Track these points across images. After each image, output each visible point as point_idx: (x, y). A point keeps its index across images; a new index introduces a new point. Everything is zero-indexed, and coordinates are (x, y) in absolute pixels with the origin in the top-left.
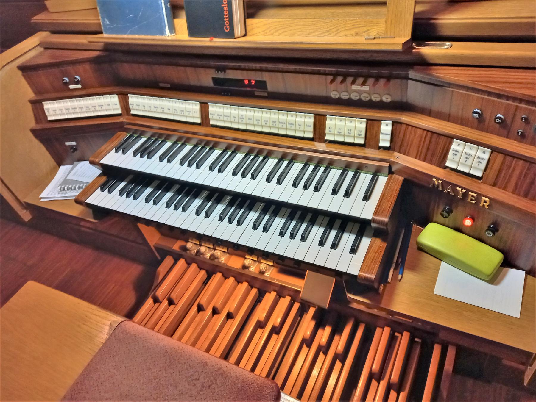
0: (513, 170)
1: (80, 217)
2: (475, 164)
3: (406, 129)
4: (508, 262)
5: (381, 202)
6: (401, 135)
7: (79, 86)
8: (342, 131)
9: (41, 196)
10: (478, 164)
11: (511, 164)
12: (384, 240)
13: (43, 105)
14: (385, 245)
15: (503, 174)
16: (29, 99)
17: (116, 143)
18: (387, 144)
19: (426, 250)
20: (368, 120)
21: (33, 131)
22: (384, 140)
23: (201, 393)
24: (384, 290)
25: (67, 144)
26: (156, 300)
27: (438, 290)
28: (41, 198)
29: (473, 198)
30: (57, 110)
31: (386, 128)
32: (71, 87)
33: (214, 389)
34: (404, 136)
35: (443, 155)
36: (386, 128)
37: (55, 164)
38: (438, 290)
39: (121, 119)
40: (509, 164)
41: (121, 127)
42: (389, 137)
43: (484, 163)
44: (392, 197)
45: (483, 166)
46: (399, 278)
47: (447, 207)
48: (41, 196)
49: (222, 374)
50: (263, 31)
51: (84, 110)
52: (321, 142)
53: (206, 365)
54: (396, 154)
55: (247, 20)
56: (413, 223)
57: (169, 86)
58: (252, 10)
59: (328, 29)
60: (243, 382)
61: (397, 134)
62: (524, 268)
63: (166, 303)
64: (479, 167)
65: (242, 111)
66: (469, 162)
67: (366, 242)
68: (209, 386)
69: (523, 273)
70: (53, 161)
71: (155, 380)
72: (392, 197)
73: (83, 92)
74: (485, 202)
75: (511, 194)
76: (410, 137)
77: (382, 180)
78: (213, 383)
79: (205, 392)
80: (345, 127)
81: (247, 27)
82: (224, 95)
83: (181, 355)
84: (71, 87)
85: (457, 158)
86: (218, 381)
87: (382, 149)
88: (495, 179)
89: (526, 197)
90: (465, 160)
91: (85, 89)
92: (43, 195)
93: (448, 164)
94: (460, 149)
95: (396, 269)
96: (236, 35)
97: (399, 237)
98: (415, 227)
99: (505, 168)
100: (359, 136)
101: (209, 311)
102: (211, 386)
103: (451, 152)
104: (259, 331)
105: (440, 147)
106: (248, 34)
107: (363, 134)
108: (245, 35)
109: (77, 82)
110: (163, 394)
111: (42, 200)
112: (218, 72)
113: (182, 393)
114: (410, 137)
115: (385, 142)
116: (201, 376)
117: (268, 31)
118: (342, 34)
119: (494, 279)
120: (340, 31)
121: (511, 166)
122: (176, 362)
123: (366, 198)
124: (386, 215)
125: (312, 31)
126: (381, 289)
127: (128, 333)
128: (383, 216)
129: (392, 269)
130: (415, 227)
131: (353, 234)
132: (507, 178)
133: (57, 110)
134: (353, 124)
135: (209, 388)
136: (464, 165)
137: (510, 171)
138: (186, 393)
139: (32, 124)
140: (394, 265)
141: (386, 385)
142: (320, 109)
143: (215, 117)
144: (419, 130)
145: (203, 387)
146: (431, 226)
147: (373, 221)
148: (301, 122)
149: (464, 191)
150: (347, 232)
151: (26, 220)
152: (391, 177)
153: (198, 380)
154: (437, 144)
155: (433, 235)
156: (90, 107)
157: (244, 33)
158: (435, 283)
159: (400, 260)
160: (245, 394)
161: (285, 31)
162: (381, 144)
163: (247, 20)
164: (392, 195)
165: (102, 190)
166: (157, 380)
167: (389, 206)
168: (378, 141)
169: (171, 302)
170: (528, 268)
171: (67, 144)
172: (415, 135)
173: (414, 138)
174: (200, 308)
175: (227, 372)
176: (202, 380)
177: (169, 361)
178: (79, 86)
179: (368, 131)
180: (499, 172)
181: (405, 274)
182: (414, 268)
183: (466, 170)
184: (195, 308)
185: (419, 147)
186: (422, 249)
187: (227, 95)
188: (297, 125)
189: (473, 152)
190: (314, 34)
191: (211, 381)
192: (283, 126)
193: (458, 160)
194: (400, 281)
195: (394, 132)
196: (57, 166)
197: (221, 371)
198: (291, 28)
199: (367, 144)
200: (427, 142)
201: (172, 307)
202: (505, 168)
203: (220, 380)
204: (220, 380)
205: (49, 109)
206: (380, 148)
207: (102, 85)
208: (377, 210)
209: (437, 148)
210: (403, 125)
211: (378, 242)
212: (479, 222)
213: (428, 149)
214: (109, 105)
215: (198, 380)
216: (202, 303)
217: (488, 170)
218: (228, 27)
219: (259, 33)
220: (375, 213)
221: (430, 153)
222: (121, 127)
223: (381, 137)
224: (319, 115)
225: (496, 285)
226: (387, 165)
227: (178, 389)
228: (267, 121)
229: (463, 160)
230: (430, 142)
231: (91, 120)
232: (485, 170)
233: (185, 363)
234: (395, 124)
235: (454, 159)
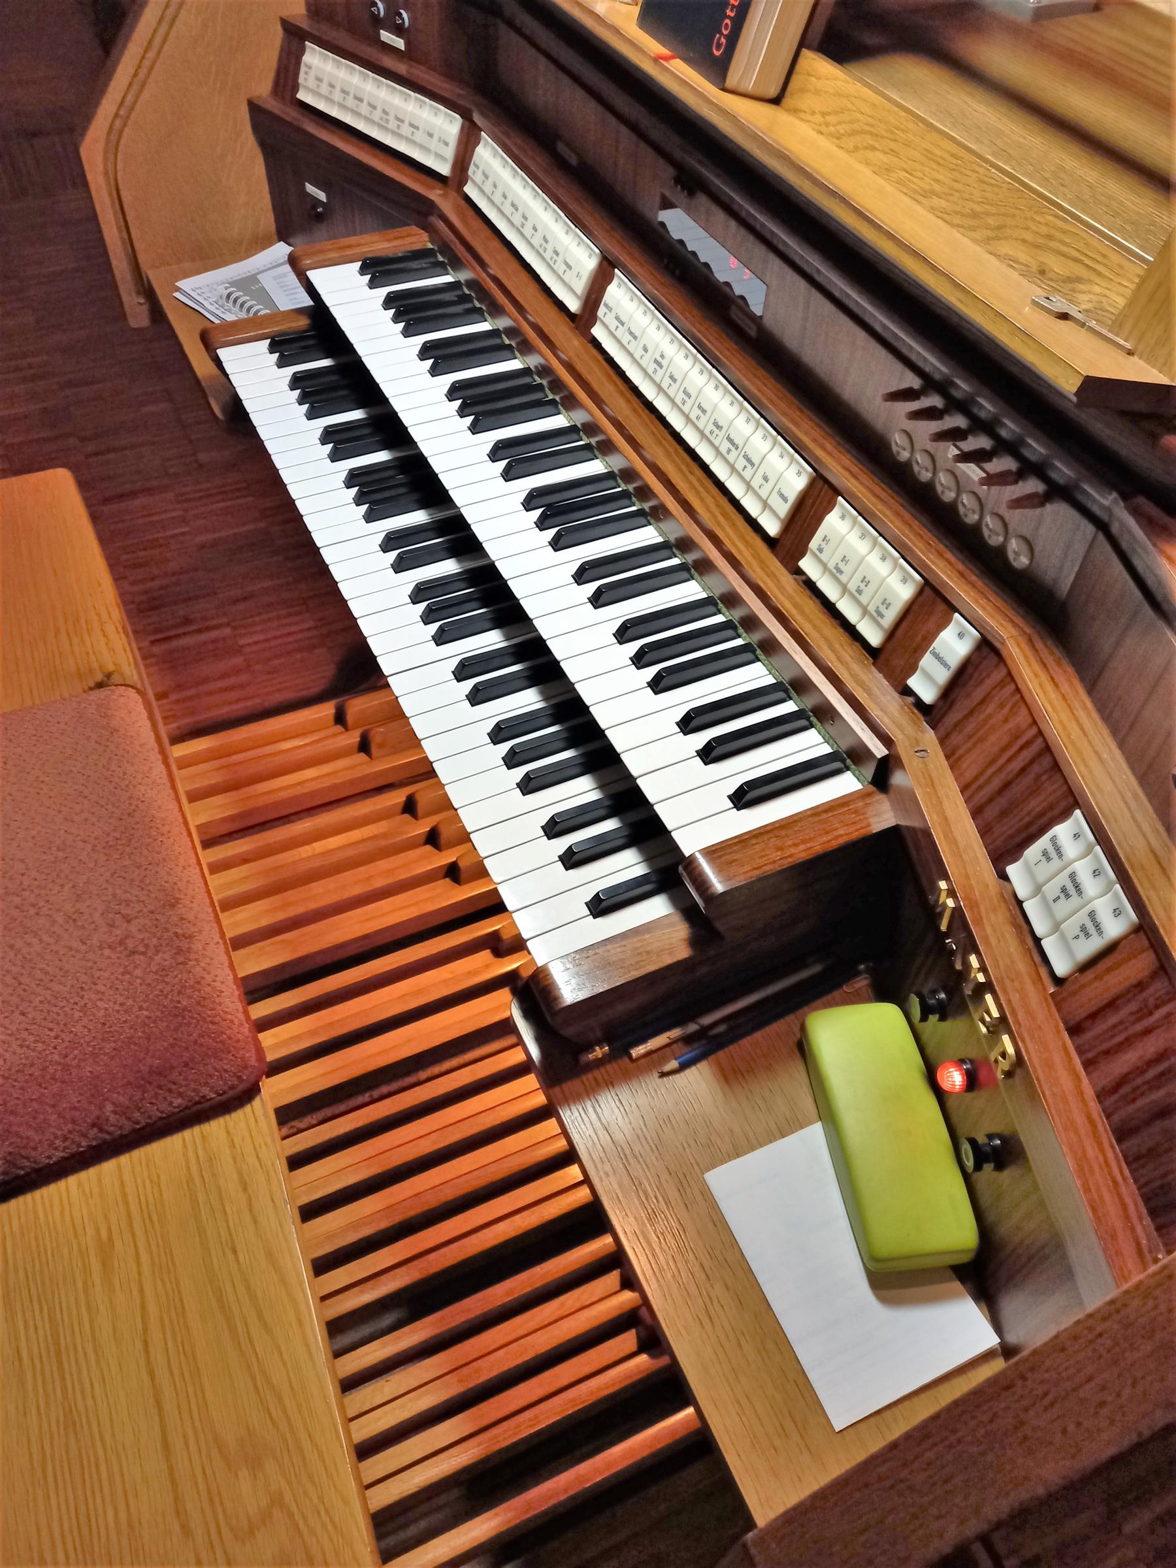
0: (1148, 1032)
1: (204, 384)
2: (1071, 927)
3: (1001, 684)
4: (983, 1274)
5: (755, 836)
6: (978, 694)
7: (400, 43)
8: (847, 569)
9: (179, 284)
10: (1077, 931)
11: (1157, 1007)
12: (695, 942)
13: (302, 51)
14: (683, 952)
15: (1113, 1019)
16: (285, 14)
17: (382, 245)
18: (928, 695)
19: (808, 1059)
20: (927, 582)
21: (254, 108)
22: (928, 676)
23: (107, 952)
24: (600, 1063)
25: (310, 188)
26: (340, 718)
27: (727, 1182)
28: (178, 289)
29: (988, 1019)
30: (334, 84)
31: (954, 643)
32: (386, 36)
33: (136, 967)
34: (982, 702)
35: (1024, 835)
36: (954, 643)
37: (273, 228)
38: (727, 1182)
39: (435, 195)
40: (1151, 1001)
41: (420, 211)
42: (942, 676)
43: (1094, 945)
44: (802, 847)
45: (1086, 949)
46: (668, 1067)
47: (943, 996)
48: (179, 284)
49: (179, 951)
50: (823, 114)
51: (377, 116)
52: (785, 567)
53: (173, 906)
54: (929, 737)
55: (805, 52)
56: (867, 971)
57: (574, 160)
58: (847, 32)
59: (978, 208)
60: (199, 1003)
61: (972, 682)
62: (1006, 1328)
63: (354, 738)
64: (1075, 944)
65: (863, 536)
66: (1063, 908)
67: (657, 908)
68: (133, 953)
69: (993, 1340)
70: (271, 217)
71: (59, 849)
72: (802, 847)
73: (402, 68)
74: (1004, 1055)
75: (1089, 1092)
76: (990, 717)
77: (846, 784)
78: (143, 953)
79: (114, 956)
80: (863, 564)
81: (794, 78)
82: (666, 268)
83: (148, 845)
84: (386, 36)
85: (1044, 871)
86: (158, 958)
87: (911, 700)
88: (1086, 1018)
89: (1119, 1140)
90: (1058, 892)
91: (411, 59)
92: (185, 284)
93: (1012, 870)
94: (1071, 849)
95: (687, 1040)
96: (732, 80)
97: (794, 971)
98: (862, 982)
99: (1133, 1007)
100: (875, 617)
101: (422, 828)
102: (136, 957)
103: (1043, 842)
104: (486, 955)
105: (1036, 804)
106: (787, 101)
107: (890, 617)
108: (776, 101)
109: (399, 31)
110: (43, 892)
111: (177, 295)
112: (676, 184)
113: (74, 921)
114: (990, 717)
115: (925, 687)
116: (142, 921)
117: (831, 119)
118: (1005, 248)
119: (897, 1279)
120: (1053, 244)
121: (1151, 1013)
122: (128, 850)
123: (743, 798)
124: (730, 879)
125: (936, 187)
126: (599, 1052)
127: (106, 716)
128: (720, 870)
129: (675, 1033)
130: (862, 982)
131: (650, 866)
132: (1118, 1039)
133: (334, 84)
134: (883, 569)
135: (128, 956)
136: (1047, 907)
137: (1139, 1027)
138: (83, 927)
139: (263, 89)
140: (692, 1028)
141: (627, 1308)
142: (841, 468)
143: (613, 324)
144: (1023, 711)
145: (121, 943)
146: (889, 1013)
147: (690, 863)
148: (764, 466)
149: (981, 978)
150: (642, 851)
151: (133, 323)
152: (869, 795)
153: (129, 921)
154: (1034, 791)
155: (859, 1039)
156: (391, 117)
157: (773, 92)
158: (738, 1155)
159: (722, 1028)
160: (176, 1030)
161: (874, 148)
162: (914, 682)
163: (805, 52)
164: (811, 840)
165: (272, 349)
166: (60, 854)
167: (774, 859)
168: (912, 669)
169: (364, 746)
170: (1012, 1338)
171: (310, 188)
172: (1006, 721)
173: (995, 732)
174: (410, 807)
175: (193, 956)
176: (133, 928)
177: (117, 835)
178: (400, 43)
179: (910, 617)
180: (1112, 1005)
181: (692, 1073)
182: (729, 1077)
183: (1040, 929)
184: (398, 797)
185: (991, 763)
186: (803, 1049)
187: (672, 274)
188: (760, 473)
189: (1091, 886)
190: (936, 201)
191: (147, 946)
192: (729, 451)
193: (1041, 878)
194: (663, 1075)
195: (970, 670)
196: (275, 237)
197: (184, 945)
198: (893, 145)
199: (882, 657)
200: (1017, 765)
201: (362, 757)
202: (1133, 1007)
203: (164, 957)
204: (164, 957)
205: (310, 67)
206: (907, 691)
207: (449, 71)
208: (723, 849)
209: (1024, 799)
210: (1002, 665)
211: (681, 931)
212: (978, 1100)
213: (1007, 785)
214: (431, 135)
215: (129, 921)
216: (418, 797)
217: (1090, 974)
218: (723, 40)
219: (813, 113)
220: (712, 852)
221: (1002, 802)
222: (420, 211)
223: (927, 661)
224: (826, 481)
225: (884, 1300)
226: (879, 750)
227: (78, 905)
228: (704, 411)
229: (1051, 889)
230: (1023, 770)
231: (366, 147)
232: (1085, 967)
233: (139, 867)
234: (985, 650)
235: (1034, 868)
